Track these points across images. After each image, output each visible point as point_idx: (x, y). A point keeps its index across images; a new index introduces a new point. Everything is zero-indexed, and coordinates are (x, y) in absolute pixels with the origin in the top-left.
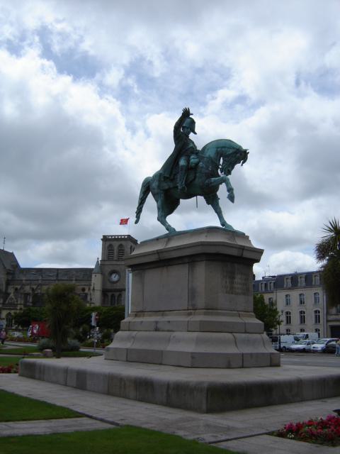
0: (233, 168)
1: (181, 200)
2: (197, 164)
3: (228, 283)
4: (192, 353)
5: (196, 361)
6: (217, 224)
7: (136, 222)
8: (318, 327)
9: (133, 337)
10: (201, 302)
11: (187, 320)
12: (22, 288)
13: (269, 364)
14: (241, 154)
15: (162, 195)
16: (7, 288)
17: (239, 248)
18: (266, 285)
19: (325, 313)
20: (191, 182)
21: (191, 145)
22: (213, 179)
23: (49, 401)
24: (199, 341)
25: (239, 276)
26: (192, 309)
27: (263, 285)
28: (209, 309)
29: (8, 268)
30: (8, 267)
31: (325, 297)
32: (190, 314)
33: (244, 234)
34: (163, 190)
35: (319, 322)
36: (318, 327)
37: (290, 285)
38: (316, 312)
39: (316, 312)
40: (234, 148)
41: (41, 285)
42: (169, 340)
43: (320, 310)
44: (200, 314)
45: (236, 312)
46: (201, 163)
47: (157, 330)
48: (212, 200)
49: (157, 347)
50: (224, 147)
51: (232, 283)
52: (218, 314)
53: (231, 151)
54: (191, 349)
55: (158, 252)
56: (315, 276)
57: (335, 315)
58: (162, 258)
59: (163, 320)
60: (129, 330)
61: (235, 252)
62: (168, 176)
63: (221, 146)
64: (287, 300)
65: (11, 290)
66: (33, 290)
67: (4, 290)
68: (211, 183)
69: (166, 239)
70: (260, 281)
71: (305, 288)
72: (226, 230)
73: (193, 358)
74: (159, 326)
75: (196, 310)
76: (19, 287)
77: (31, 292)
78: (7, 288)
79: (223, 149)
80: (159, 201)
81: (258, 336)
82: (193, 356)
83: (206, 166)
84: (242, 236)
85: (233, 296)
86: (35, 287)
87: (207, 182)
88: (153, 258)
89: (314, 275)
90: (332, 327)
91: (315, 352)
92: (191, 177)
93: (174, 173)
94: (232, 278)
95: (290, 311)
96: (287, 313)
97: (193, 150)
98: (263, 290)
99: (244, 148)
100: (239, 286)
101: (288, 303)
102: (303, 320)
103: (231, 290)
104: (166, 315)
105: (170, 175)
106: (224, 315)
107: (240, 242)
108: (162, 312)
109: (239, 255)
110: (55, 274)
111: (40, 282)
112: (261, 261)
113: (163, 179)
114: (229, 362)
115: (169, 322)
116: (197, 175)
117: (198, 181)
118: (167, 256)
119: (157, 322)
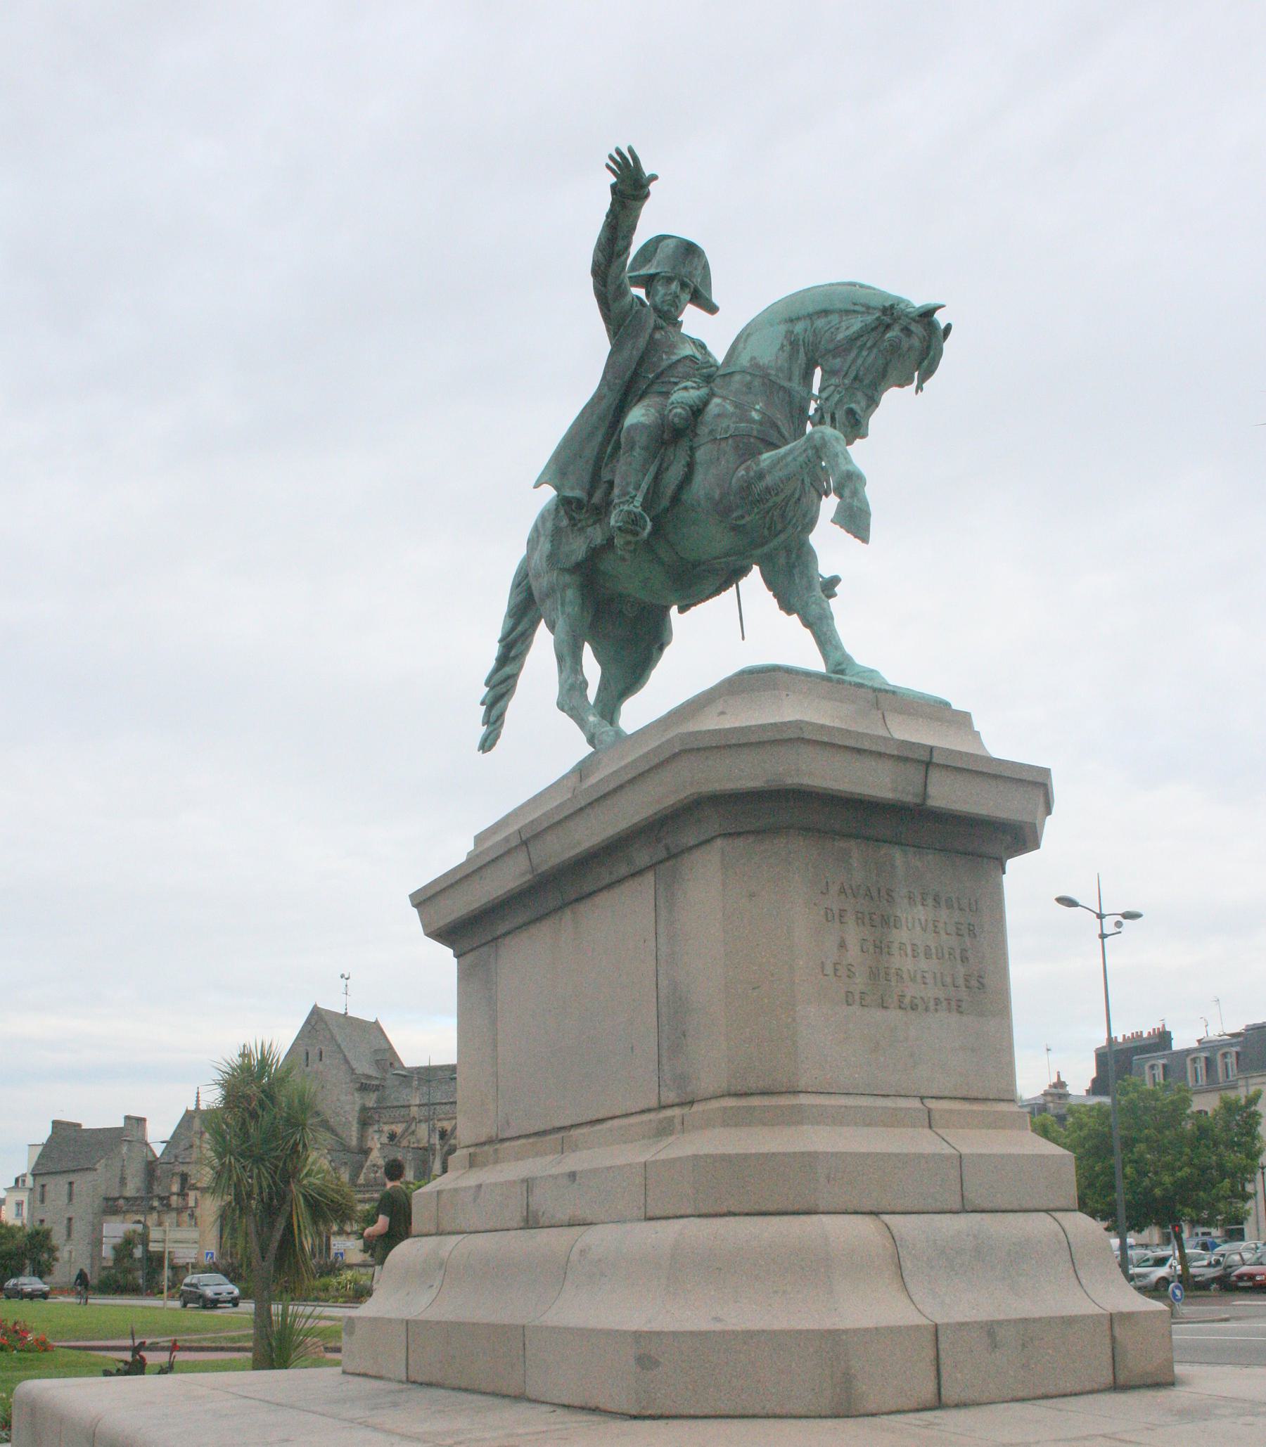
0: (873, 402)
2: (697, 411)
4: (638, 1336)
6: (809, 658)
7: (487, 744)
9: (442, 1265)
11: (647, 1156)
13: (1106, 1377)
14: (907, 331)
15: (570, 594)
16: (362, 1138)
17: (899, 759)
18: (1209, 1062)
20: (676, 499)
22: (765, 456)
23: (791, 781)
26: (677, 1103)
27: (1201, 1065)
30: (364, 1067)
32: (664, 1130)
33: (947, 705)
40: (868, 309)
47: (530, 1222)
48: (800, 590)
50: (825, 312)
51: (881, 948)
52: (796, 1117)
53: (856, 324)
58: (856, 852)
59: (554, 1171)
61: (878, 783)
62: (578, 493)
65: (376, 1142)
67: (354, 1142)
68: (761, 476)
70: (1188, 1052)
72: (840, 675)
73: (646, 1362)
75: (692, 1103)
76: (399, 1129)
78: (362, 1138)
79: (820, 323)
80: (560, 623)
81: (1041, 1225)
82: (647, 1351)
84: (937, 711)
85: (894, 1015)
87: (741, 472)
92: (674, 475)
93: (606, 475)
98: (1202, 1080)
100: (923, 964)
103: (879, 987)
104: (575, 1148)
105: (590, 495)
106: (838, 1118)
108: (555, 1135)
109: (908, 797)
112: (1044, 842)
114: (848, 1379)
115: (572, 1176)
117: (704, 485)
118: (557, 851)
119: (528, 1184)
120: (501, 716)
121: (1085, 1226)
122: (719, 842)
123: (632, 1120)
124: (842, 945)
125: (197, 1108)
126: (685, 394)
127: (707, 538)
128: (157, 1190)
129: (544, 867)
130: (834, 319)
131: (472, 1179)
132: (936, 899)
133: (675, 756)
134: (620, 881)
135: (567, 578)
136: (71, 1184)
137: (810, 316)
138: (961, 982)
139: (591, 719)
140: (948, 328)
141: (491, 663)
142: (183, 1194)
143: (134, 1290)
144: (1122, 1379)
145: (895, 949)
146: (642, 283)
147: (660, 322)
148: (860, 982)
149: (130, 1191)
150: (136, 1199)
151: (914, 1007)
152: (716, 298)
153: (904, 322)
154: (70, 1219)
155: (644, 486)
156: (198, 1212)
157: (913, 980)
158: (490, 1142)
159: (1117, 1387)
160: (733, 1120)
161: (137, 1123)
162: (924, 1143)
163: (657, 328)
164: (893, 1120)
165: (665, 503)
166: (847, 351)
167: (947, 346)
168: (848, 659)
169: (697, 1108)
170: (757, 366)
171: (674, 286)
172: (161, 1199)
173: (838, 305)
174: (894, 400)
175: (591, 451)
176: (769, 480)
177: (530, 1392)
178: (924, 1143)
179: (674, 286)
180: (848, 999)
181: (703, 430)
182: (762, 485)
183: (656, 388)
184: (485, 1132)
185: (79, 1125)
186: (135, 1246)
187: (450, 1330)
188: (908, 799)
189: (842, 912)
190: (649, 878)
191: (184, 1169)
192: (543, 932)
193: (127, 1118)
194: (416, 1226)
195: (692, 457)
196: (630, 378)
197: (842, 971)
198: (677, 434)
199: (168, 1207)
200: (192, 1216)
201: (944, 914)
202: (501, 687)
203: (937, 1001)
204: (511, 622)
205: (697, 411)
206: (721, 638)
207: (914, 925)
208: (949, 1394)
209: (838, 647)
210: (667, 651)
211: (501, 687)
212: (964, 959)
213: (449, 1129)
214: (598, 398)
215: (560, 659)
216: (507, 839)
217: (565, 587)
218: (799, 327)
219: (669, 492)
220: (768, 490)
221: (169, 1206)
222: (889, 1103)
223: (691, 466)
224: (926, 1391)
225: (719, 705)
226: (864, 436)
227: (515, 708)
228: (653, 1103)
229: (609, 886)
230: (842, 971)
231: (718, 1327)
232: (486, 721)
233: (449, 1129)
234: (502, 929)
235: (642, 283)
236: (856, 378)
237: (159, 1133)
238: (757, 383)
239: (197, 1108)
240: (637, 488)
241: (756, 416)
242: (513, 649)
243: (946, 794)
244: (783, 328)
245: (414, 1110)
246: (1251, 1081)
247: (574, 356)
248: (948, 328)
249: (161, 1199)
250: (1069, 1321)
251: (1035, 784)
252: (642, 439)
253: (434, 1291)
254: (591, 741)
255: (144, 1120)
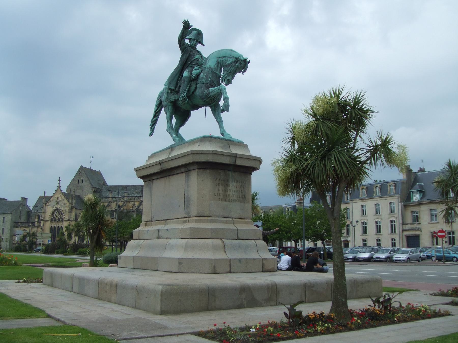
0: (233, 77)
1: (192, 111)
2: (198, 75)
3: (221, 192)
4: (179, 259)
5: (215, 268)
6: (217, 134)
7: (151, 135)
8: (393, 236)
9: (140, 246)
10: (194, 210)
12: (108, 205)
14: (241, 63)
15: (170, 107)
17: (230, 156)
19: (401, 222)
20: (193, 93)
21: (197, 56)
22: (211, 89)
23: (211, 160)
24: (187, 248)
25: (234, 184)
26: (187, 217)
28: (201, 216)
29: (94, 186)
31: (400, 205)
32: (185, 222)
33: (242, 143)
34: (171, 102)
35: (395, 232)
36: (393, 236)
37: (379, 194)
38: (391, 221)
39: (391, 221)
40: (234, 57)
41: (126, 201)
42: (165, 248)
43: (395, 219)
44: (193, 222)
45: (231, 219)
46: (202, 74)
47: (159, 238)
49: (155, 254)
50: (225, 57)
51: (226, 191)
53: (231, 60)
54: (209, 255)
55: (160, 163)
56: (390, 186)
57: (410, 224)
58: (222, 173)
59: (164, 228)
60: (139, 239)
61: (227, 160)
62: (173, 88)
63: (222, 56)
64: (376, 209)
66: (119, 206)
68: (210, 93)
69: (170, 150)
71: (380, 197)
73: (180, 263)
74: (161, 234)
75: (190, 217)
77: (116, 208)
79: (224, 59)
80: (168, 113)
82: (181, 261)
83: (206, 76)
84: (241, 144)
85: (228, 203)
86: (120, 204)
88: (156, 169)
89: (388, 185)
90: (408, 237)
91: (398, 261)
92: (193, 88)
93: (179, 85)
94: (226, 185)
95: (366, 221)
96: (363, 223)
97: (200, 62)
99: (245, 57)
101: (364, 212)
102: (378, 229)
103: (225, 198)
105: (175, 88)
107: (235, 150)
110: (140, 190)
111: (126, 199)
113: (170, 92)
115: (167, 230)
116: (198, 85)
117: (198, 92)
119: (158, 230)
120: (154, 129)
121: (263, 243)
122: (197, 170)
123: (179, 219)
124: (219, 190)
125: (44, 196)
126: (196, 71)
127: (198, 101)
128: (31, 220)
129: (164, 169)
130: (227, 58)
131: (147, 228)
132: (237, 181)
133: (190, 154)
134: (179, 173)
135: (169, 104)
136: (4, 218)
137: (222, 57)
138: (241, 197)
139: (174, 135)
140: (249, 61)
141: (152, 117)
142: (39, 222)
143: (26, 251)
144: (264, 270)
145: (229, 191)
146: (189, 38)
147: (192, 50)
148: (221, 197)
149: (22, 221)
150: (24, 223)
151: (231, 201)
152: (204, 43)
153: (240, 61)
154: (3, 229)
155: (187, 90)
156: (43, 228)
157: (232, 196)
158: (150, 221)
159: (263, 271)
160: (197, 221)
161: (25, 199)
162: (231, 227)
163: (191, 51)
164: (226, 222)
165: (191, 93)
166: (229, 66)
167: (249, 65)
168: (224, 131)
169: (191, 218)
170: (210, 67)
171: (195, 41)
172: (32, 223)
173: (227, 55)
174: (238, 75)
175: (176, 79)
176: (211, 94)
177: (159, 269)
178: (231, 227)
179: (195, 41)
180: (219, 200)
181: (199, 80)
182: (210, 95)
183: (190, 65)
184: (149, 219)
185: (6, 200)
186: (27, 237)
187: (142, 258)
188: (232, 163)
189: (219, 184)
190: (184, 174)
191: (39, 214)
192: (163, 180)
193: (22, 198)
194: (134, 237)
195: (196, 86)
196: (185, 64)
197: (218, 195)
198: (194, 80)
199: (34, 226)
200: (42, 229)
201: (238, 184)
202: (154, 122)
203: (236, 200)
204: (157, 108)
205: (198, 75)
206: (200, 122)
207: (233, 186)
208: (232, 271)
209: (223, 128)
210: (190, 118)
211: (154, 122)
212: (242, 192)
213: (121, 205)
214: (178, 67)
215: (168, 121)
216: (156, 162)
217: (169, 106)
218: (219, 59)
219: (192, 91)
220: (211, 96)
221: (34, 225)
222: (226, 219)
223: (196, 88)
224: (228, 270)
225: (198, 144)
226: (231, 84)
227: (157, 127)
228: (183, 217)
229: (177, 174)
230: (218, 195)
231: (193, 258)
232: (151, 130)
233: (121, 205)
234: (154, 178)
235: (189, 38)
236: (230, 72)
237: (31, 203)
238: (210, 71)
239: (44, 196)
240: (185, 90)
241: (209, 79)
242: (157, 114)
243: (239, 162)
244: (216, 59)
245: (110, 199)
246: (353, 202)
247: (173, 58)
248: (249, 61)
249: (32, 223)
250: (254, 259)
251: (259, 161)
252: (186, 80)
253: (138, 251)
254: (174, 140)
255: (27, 199)
